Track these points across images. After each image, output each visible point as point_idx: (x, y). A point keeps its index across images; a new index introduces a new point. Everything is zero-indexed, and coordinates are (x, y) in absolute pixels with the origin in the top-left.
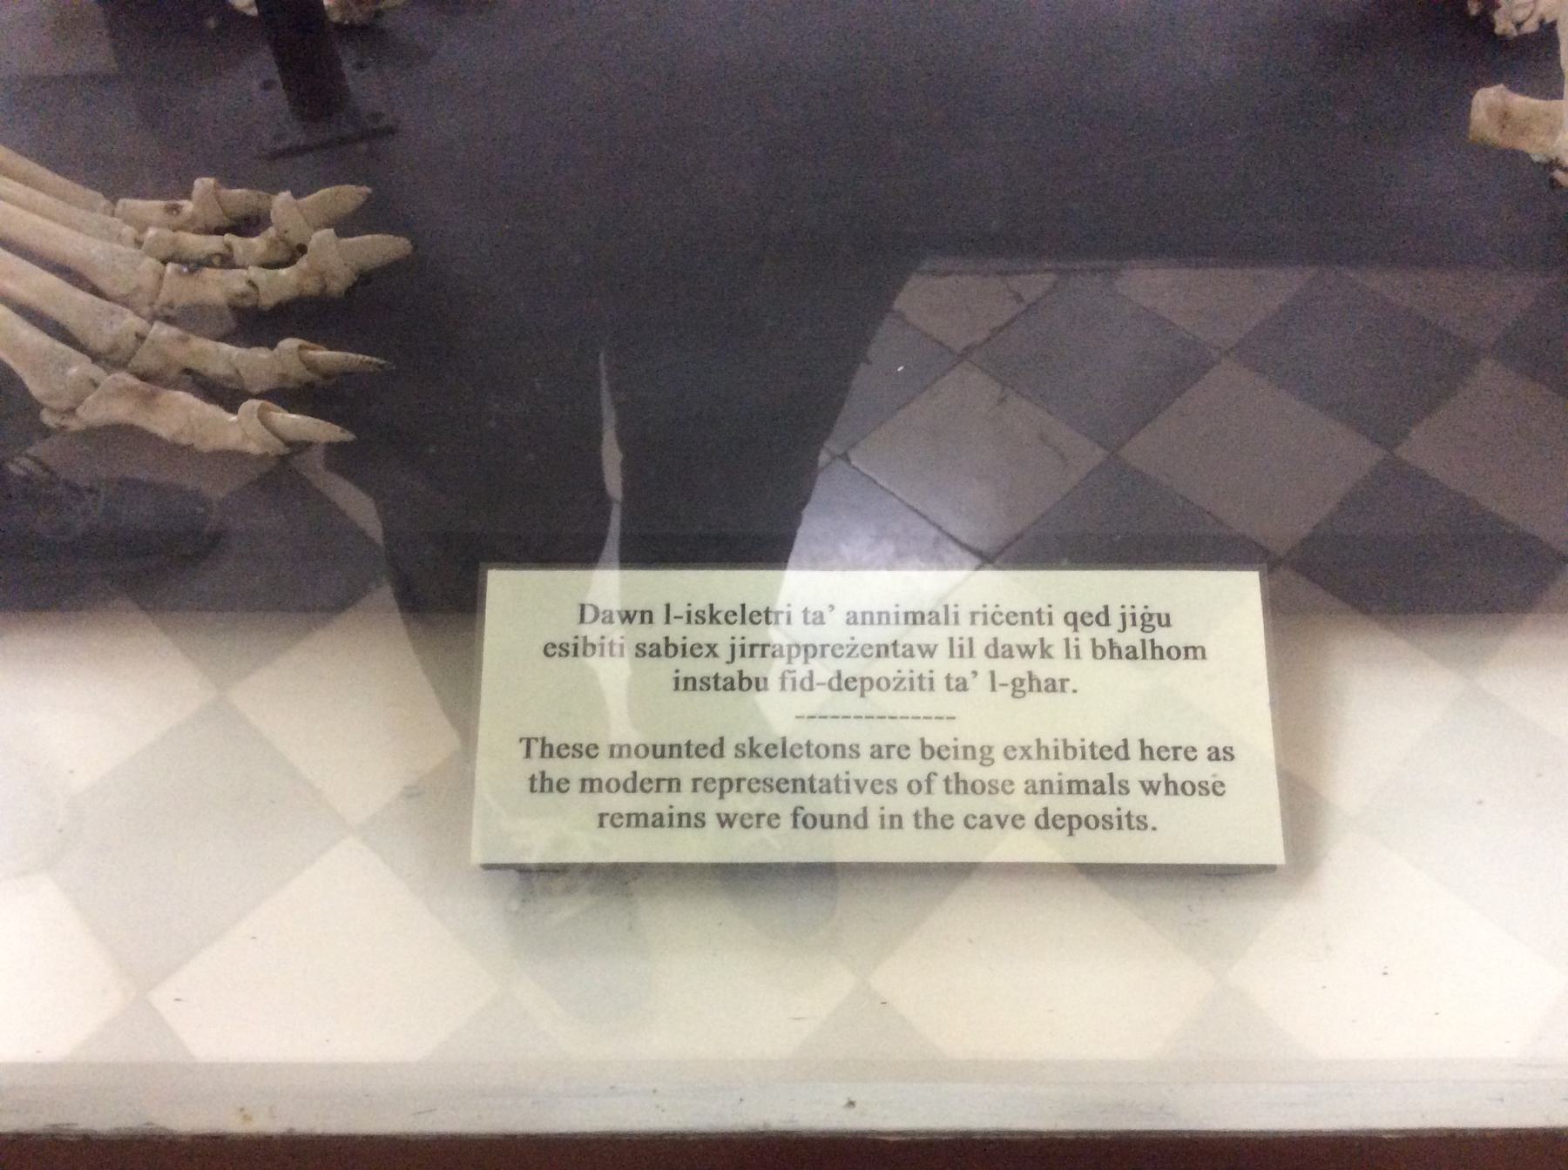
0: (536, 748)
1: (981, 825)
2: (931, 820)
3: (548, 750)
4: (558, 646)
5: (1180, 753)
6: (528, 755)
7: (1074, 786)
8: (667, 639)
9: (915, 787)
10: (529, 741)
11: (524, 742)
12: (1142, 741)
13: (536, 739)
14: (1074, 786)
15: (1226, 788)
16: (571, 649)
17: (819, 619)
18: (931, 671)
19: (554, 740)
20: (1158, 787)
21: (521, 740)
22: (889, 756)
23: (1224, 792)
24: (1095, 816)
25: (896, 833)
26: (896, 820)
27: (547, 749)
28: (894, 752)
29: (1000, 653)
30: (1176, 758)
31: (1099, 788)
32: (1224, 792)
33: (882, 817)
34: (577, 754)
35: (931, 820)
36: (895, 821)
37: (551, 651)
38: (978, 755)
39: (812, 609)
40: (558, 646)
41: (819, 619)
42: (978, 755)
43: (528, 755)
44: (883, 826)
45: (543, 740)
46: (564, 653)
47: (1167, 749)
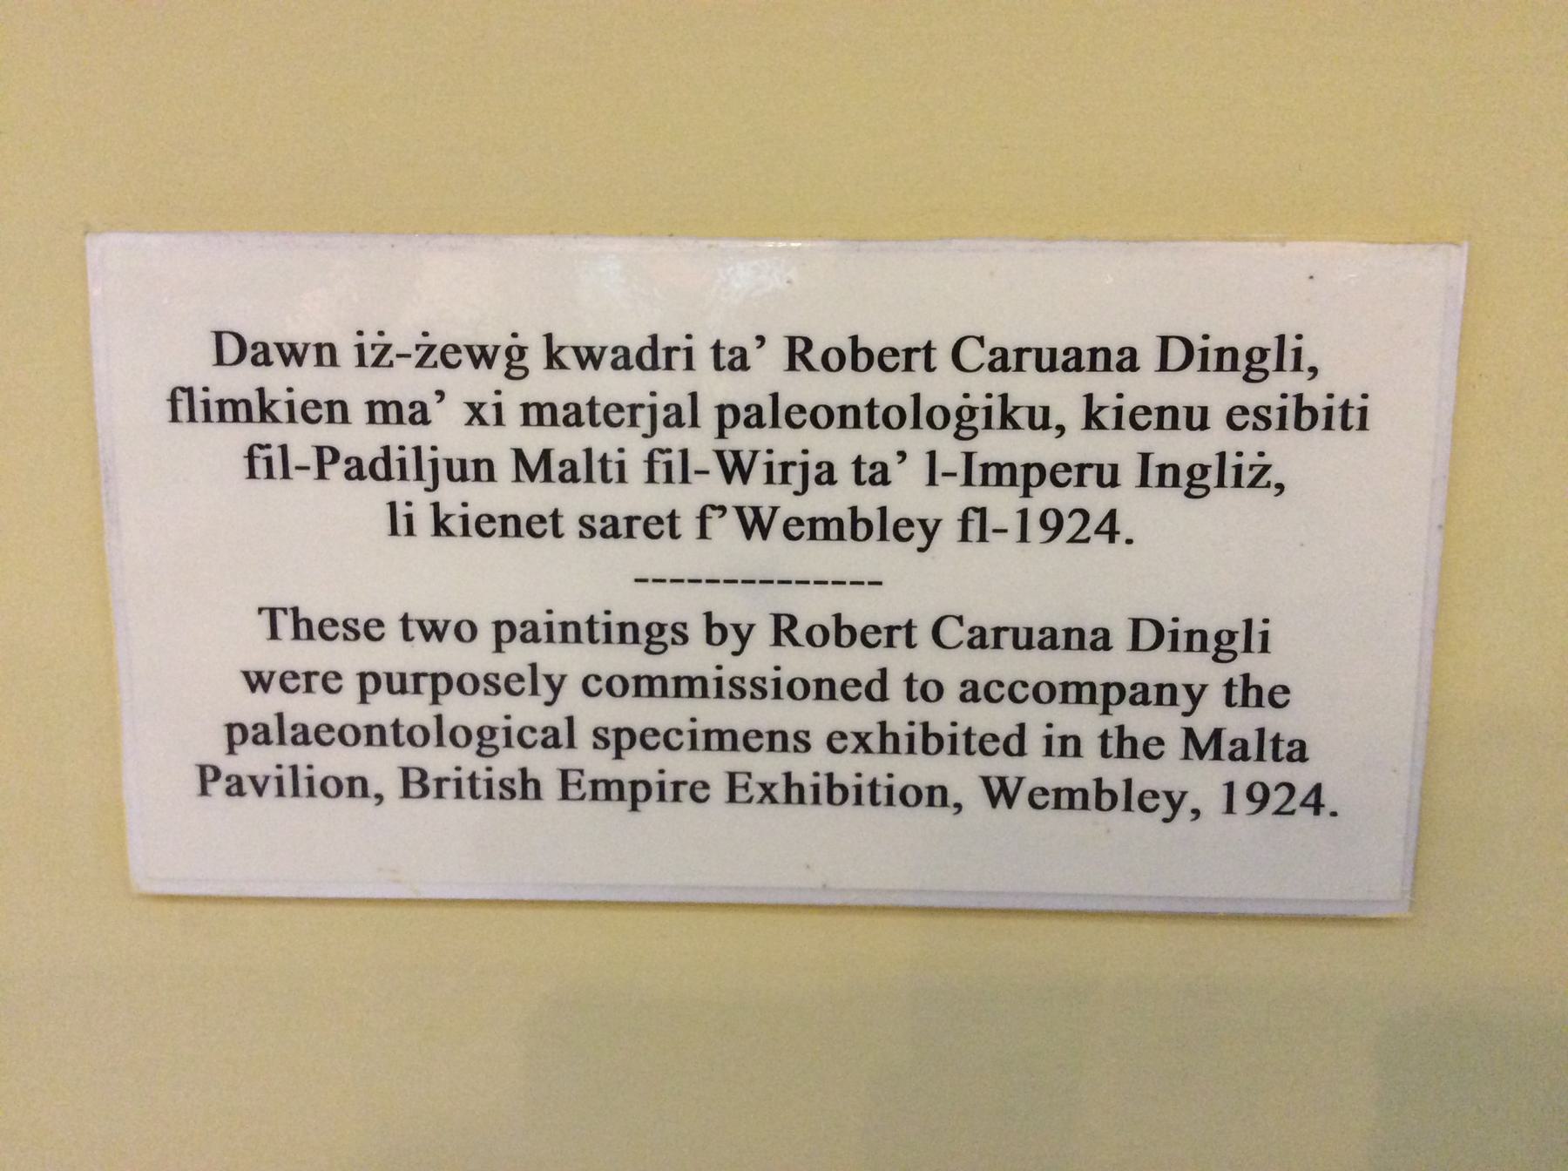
0: (285, 624)
1: (992, 367)
2: (1127, 745)
3: (305, 628)
4: (1251, 410)
5: (316, 682)
6: (274, 635)
7: (714, 738)
8: (855, 339)
9: (932, 691)
10: (273, 612)
11: (266, 614)
12: (709, 615)
13: (285, 610)
14: (714, 738)
15: (711, 792)
16: (1274, 417)
17: (741, 361)
18: (621, 450)
19: (314, 611)
20: (265, 785)
21: (260, 610)
22: (997, 645)
23: (708, 797)
24: (1263, 785)
25: (531, 806)
26: (1071, 744)
27: (303, 626)
28: (1029, 360)
29: (1059, 364)
30: (309, 689)
31: (642, 739)
32: (708, 797)
33: (1049, 739)
34: (351, 635)
35: (1127, 745)
36: (1070, 746)
37: (1239, 420)
38: (643, 636)
39: (727, 343)
40: (1251, 410)
41: (741, 361)
42: (643, 636)
43: (274, 635)
44: (1049, 753)
45: (295, 610)
46: (1261, 424)
47: (295, 676)
